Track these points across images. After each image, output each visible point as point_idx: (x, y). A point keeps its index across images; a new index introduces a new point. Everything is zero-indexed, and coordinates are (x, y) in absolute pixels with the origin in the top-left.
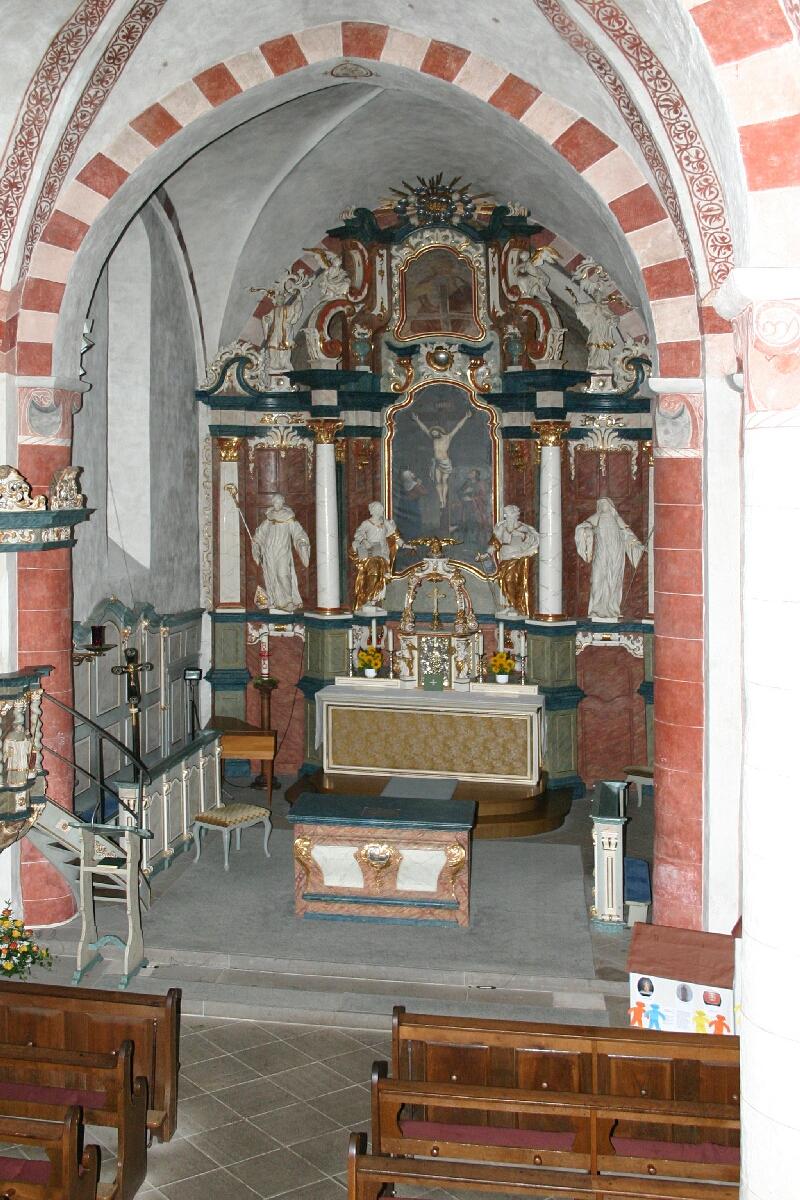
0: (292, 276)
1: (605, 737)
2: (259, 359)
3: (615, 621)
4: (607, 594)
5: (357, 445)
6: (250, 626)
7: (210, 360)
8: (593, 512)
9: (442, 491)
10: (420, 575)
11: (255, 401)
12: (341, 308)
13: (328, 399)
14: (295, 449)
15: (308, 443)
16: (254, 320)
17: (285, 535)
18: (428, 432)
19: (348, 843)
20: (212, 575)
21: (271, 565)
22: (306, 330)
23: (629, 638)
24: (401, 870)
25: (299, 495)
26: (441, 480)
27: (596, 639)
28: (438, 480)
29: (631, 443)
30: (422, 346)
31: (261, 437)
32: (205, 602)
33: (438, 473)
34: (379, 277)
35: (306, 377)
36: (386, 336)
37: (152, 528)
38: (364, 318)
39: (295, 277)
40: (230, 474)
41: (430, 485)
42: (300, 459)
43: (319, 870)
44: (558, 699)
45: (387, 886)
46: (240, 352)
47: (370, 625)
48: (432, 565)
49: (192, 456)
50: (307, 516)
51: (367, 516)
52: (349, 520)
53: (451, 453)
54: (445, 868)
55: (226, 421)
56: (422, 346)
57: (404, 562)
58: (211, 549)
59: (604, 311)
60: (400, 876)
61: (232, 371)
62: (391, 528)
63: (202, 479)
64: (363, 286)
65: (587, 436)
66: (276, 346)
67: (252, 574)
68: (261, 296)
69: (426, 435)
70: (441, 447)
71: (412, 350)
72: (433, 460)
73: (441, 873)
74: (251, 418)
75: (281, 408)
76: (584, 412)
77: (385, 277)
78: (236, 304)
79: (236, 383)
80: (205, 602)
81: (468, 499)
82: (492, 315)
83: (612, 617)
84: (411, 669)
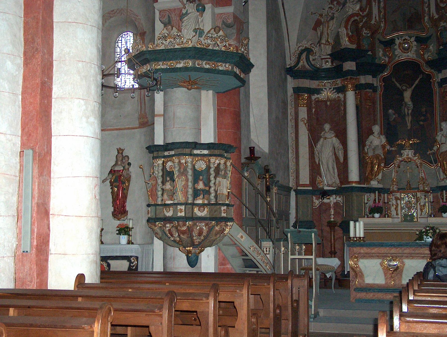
0: (330, 6)
2: (316, 49)
6: (314, 198)
10: (400, 159)
11: (315, 74)
12: (356, 18)
14: (334, 100)
15: (341, 96)
18: (400, 87)
21: (324, 163)
22: (340, 30)
26: (408, 113)
28: (406, 113)
30: (396, 39)
31: (318, 94)
32: (292, 184)
33: (406, 110)
34: (374, 3)
35: (339, 55)
36: (378, 36)
37: (269, 133)
38: (367, 25)
39: (332, 6)
40: (303, 113)
41: (403, 117)
43: (362, 274)
46: (307, 46)
47: (375, 193)
48: (406, 153)
49: (285, 103)
50: (342, 135)
52: (363, 135)
53: (412, 98)
55: (301, 85)
56: (396, 39)
57: (388, 159)
58: (294, 156)
61: (304, 56)
62: (383, 140)
63: (289, 118)
64: (366, 7)
66: (324, 42)
67: (315, 169)
69: (398, 88)
70: (407, 95)
71: (392, 41)
72: (403, 102)
74: (314, 84)
75: (328, 78)
77: (377, 4)
79: (306, 63)
81: (421, 123)
82: (431, 18)
84: (397, 211)
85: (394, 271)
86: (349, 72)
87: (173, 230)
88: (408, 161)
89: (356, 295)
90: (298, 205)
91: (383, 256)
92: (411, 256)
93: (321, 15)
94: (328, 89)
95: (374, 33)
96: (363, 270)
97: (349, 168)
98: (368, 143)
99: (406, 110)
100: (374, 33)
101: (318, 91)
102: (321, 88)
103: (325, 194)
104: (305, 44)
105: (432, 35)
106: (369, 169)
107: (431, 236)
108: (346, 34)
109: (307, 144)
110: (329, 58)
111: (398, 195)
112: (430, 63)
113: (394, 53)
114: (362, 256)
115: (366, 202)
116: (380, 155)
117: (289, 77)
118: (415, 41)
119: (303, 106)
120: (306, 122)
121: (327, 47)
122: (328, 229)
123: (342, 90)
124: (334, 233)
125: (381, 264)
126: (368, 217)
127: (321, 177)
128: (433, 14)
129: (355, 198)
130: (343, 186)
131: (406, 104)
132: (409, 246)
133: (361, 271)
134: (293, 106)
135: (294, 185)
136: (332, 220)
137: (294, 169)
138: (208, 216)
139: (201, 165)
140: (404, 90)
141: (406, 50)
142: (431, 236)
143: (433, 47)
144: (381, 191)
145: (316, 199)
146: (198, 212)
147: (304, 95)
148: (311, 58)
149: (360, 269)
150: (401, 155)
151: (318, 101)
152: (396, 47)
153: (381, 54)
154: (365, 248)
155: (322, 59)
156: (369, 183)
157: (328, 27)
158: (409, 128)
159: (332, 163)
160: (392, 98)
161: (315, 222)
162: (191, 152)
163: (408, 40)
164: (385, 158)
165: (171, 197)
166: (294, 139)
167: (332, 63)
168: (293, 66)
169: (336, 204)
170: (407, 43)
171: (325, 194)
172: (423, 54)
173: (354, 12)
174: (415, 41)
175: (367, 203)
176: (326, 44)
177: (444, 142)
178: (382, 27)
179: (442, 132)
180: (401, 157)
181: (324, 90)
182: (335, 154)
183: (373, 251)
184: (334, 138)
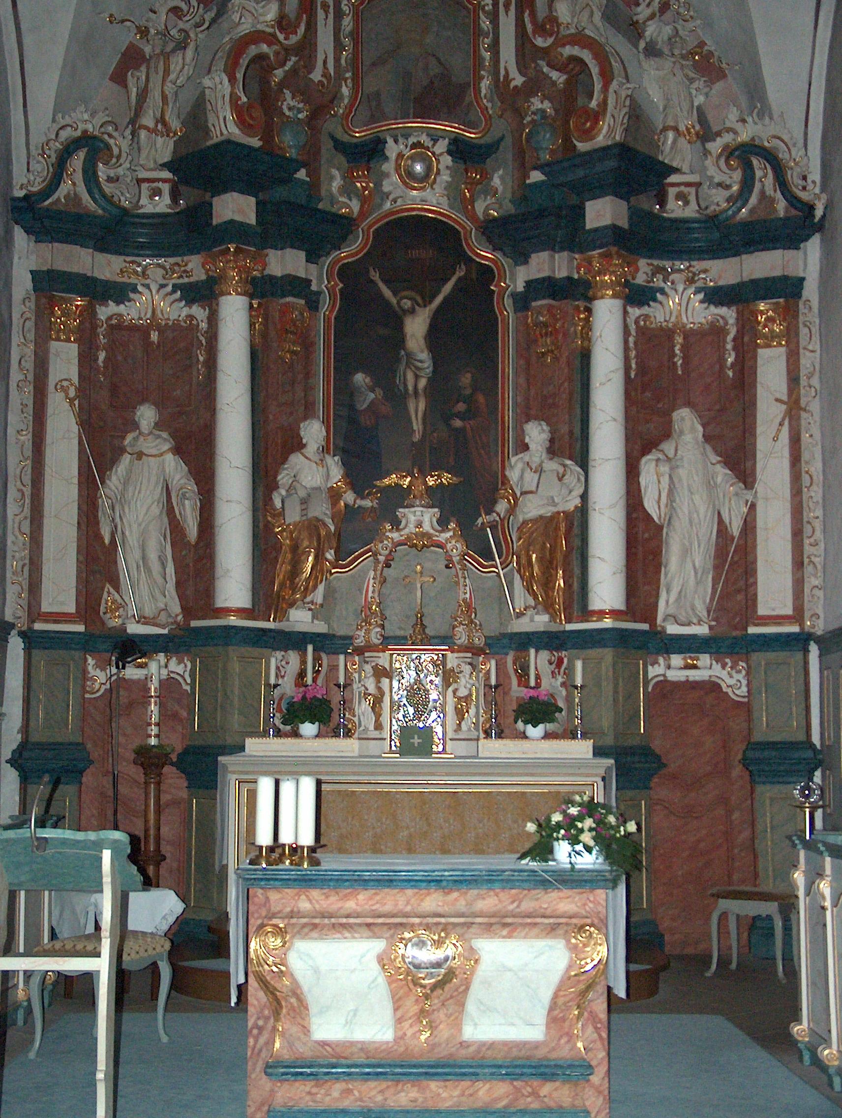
1: (686, 854)
2: (120, 143)
3: (702, 630)
4: (692, 578)
5: (283, 313)
6: (90, 661)
7: (37, 139)
8: (667, 435)
10: (395, 536)
11: (114, 230)
12: (264, 48)
13: (241, 211)
14: (176, 326)
15: (199, 313)
16: (109, 88)
17: (157, 483)
18: (394, 301)
19: (366, 932)
20: (27, 561)
21: (132, 539)
22: (207, 82)
23: (724, 667)
24: (476, 991)
25: (180, 413)
27: (672, 669)
28: (410, 388)
29: (723, 311)
30: (390, 141)
31: (118, 302)
32: (14, 610)
33: (410, 376)
34: (321, 14)
35: (200, 167)
36: (331, 126)
38: (296, 81)
40: (65, 362)
41: (397, 398)
42: (182, 345)
44: (633, 765)
45: (444, 1032)
46: (90, 128)
48: (412, 518)
50: (197, 448)
51: (299, 446)
54: (566, 980)
55: (61, 265)
56: (390, 141)
57: (350, 536)
58: (27, 511)
59: (686, 71)
60: (471, 1006)
61: (77, 161)
62: (336, 473)
63: (15, 376)
64: (299, 18)
65: (655, 300)
66: (151, 125)
67: (98, 562)
68: (127, 37)
69: (388, 304)
70: (416, 328)
73: (556, 996)
74: (107, 267)
75: (158, 249)
76: (650, 258)
77: (331, 16)
78: (83, 43)
80: (14, 610)
81: (458, 423)
82: (501, 86)
83: (700, 622)
84: (378, 715)
85: (434, 987)
86: (234, 230)
88: (421, 543)
89: (272, 1092)
90: (34, 685)
91: (392, 926)
92: (502, 924)
93: (144, 32)
94: (154, 288)
95: (318, 112)
96: (305, 988)
97: (624, 463)
98: (284, 478)
99: (410, 376)
100: (318, 112)
101: (120, 292)
102: (133, 280)
103: (129, 649)
104: (85, 121)
105: (502, 138)
106: (282, 570)
107: (591, 843)
108: (227, 98)
109: (75, 471)
110: (165, 181)
111: (383, 659)
112: (495, 231)
113: (379, 185)
114: (304, 926)
115: (272, 681)
116: (325, 524)
117: (19, 234)
118: (449, 152)
119: (68, 340)
120: (72, 393)
121: (160, 140)
122: (136, 772)
123: (204, 293)
124: (158, 792)
125: (383, 961)
126: (278, 734)
127: (117, 588)
129: (236, 666)
130: (194, 624)
131: (409, 355)
132: (497, 885)
133: (296, 992)
134: (31, 336)
135: (20, 613)
136: (153, 741)
137: (22, 559)
140: (405, 312)
141: (418, 181)
142: (591, 843)
143: (502, 178)
144: (326, 643)
145: (97, 666)
147: (70, 301)
148: (102, 171)
149: (295, 981)
150: (396, 524)
151: (118, 327)
152: (388, 167)
153: (337, 184)
154: (315, 893)
155: (139, 181)
156: (281, 615)
157: (167, 72)
158: (417, 437)
159: (157, 546)
160: (365, 332)
161: (89, 746)
163: (428, 149)
164: (338, 534)
166: (29, 453)
167: (175, 195)
168: (40, 192)
169: (169, 685)
170: (424, 159)
171: (129, 649)
172: (472, 201)
173: (260, 27)
175: (276, 686)
176: (154, 131)
177: (534, 489)
178: (342, 98)
179: (526, 456)
180: (398, 530)
181: (140, 288)
182: (170, 511)
183: (351, 905)
184: (170, 457)
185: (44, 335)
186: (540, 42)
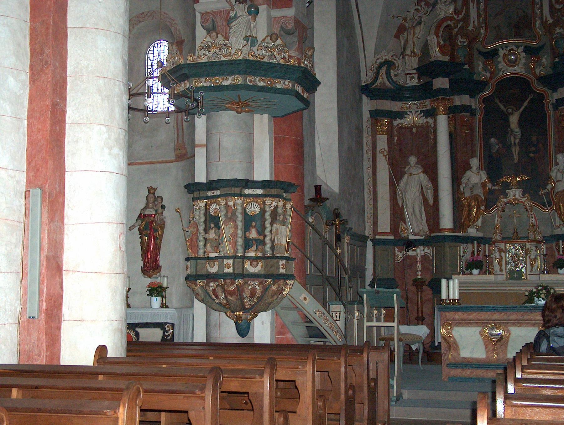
0: (417, 7)
2: (398, 62)
6: (396, 249)
9: (516, 150)
10: (505, 200)
11: (398, 93)
12: (449, 22)
14: (422, 126)
15: (430, 121)
18: (505, 110)
21: (409, 205)
22: (429, 38)
26: (515, 143)
28: (513, 143)
30: (500, 49)
31: (401, 119)
32: (368, 232)
33: (512, 139)
34: (471, 4)
35: (428, 69)
36: (477, 46)
37: (339, 167)
38: (463, 32)
39: (419, 8)
40: (382, 142)
41: (508, 147)
43: (457, 345)
46: (387, 58)
47: (473, 244)
48: (512, 193)
49: (360, 130)
50: (431, 171)
52: (458, 170)
53: (520, 123)
55: (380, 108)
56: (500, 49)
57: (490, 200)
58: (372, 197)
61: (383, 70)
62: (484, 176)
63: (365, 148)
64: (462, 9)
66: (409, 53)
67: (397, 213)
69: (503, 111)
70: (514, 119)
71: (495, 52)
72: (509, 129)
74: (396, 106)
75: (413, 98)
77: (475, 5)
79: (385, 80)
81: (532, 155)
82: (544, 23)
84: (501, 266)
85: (497, 342)
86: (441, 91)
87: (219, 290)
88: (515, 203)
89: (449, 373)
90: (377, 258)
91: (483, 323)
92: (519, 323)
93: (405, 19)
94: (413, 112)
95: (472, 41)
96: (458, 341)
98: (464, 180)
99: (512, 139)
100: (472, 41)
101: (401, 115)
102: (406, 110)
103: (410, 244)
104: (385, 56)
105: (545, 44)
106: (465, 213)
107: (544, 297)
108: (436, 43)
109: (388, 181)
110: (415, 74)
111: (502, 246)
112: (542, 80)
113: (497, 67)
114: (457, 323)
115: (462, 254)
116: (480, 196)
117: (364, 97)
118: (524, 51)
119: (383, 134)
120: (386, 154)
121: (413, 59)
122: (413, 289)
123: (431, 113)
124: (421, 294)
125: (481, 333)
126: (464, 274)
127: (405, 223)
128: (546, 18)
129: (448, 249)
130: (433, 235)
131: (512, 131)
132: (515, 310)
133: (455, 342)
134: (370, 133)
135: (371, 233)
136: (419, 277)
137: (371, 213)
138: (263, 273)
139: (254, 208)
140: (510, 114)
141: (513, 63)
142: (544, 297)
143: (546, 59)
144: (481, 241)
145: (399, 251)
146: (250, 268)
147: (384, 120)
148: (393, 73)
149: (455, 339)
150: (506, 195)
151: (401, 128)
152: (500, 59)
153: (480, 68)
154: (460, 313)
155: (406, 74)
156: (465, 230)
157: (414, 34)
158: (516, 161)
159: (418, 206)
160: (495, 123)
161: (397, 279)
162: (241, 191)
163: (515, 51)
164: (486, 200)
165: (216, 248)
166: (371, 175)
167: (419, 79)
168: (370, 84)
169: (424, 257)
171: (410, 244)
172: (534, 69)
173: (447, 15)
174: (524, 51)
175: (463, 256)
176: (411, 56)
177: (561, 179)
178: (481, 34)
179: (558, 167)
180: (506, 198)
181: (408, 113)
182: (423, 194)
183: (471, 317)
184: (422, 174)
185: (374, 134)
186: (558, 7)
